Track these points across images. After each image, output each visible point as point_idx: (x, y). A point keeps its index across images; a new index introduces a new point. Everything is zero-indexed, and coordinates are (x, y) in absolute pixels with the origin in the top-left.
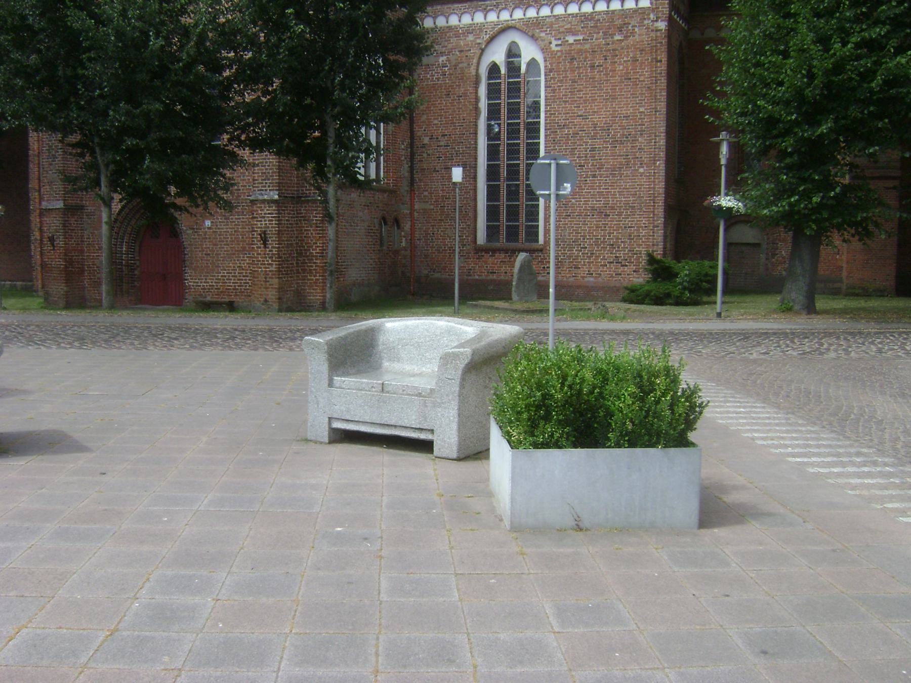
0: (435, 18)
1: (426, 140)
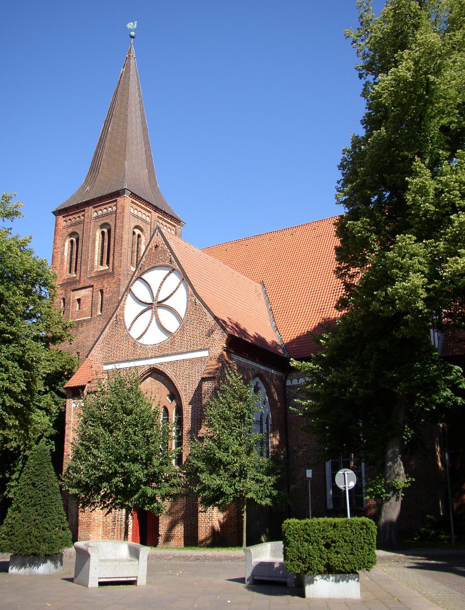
0: (298, 379)
1: (296, 448)
